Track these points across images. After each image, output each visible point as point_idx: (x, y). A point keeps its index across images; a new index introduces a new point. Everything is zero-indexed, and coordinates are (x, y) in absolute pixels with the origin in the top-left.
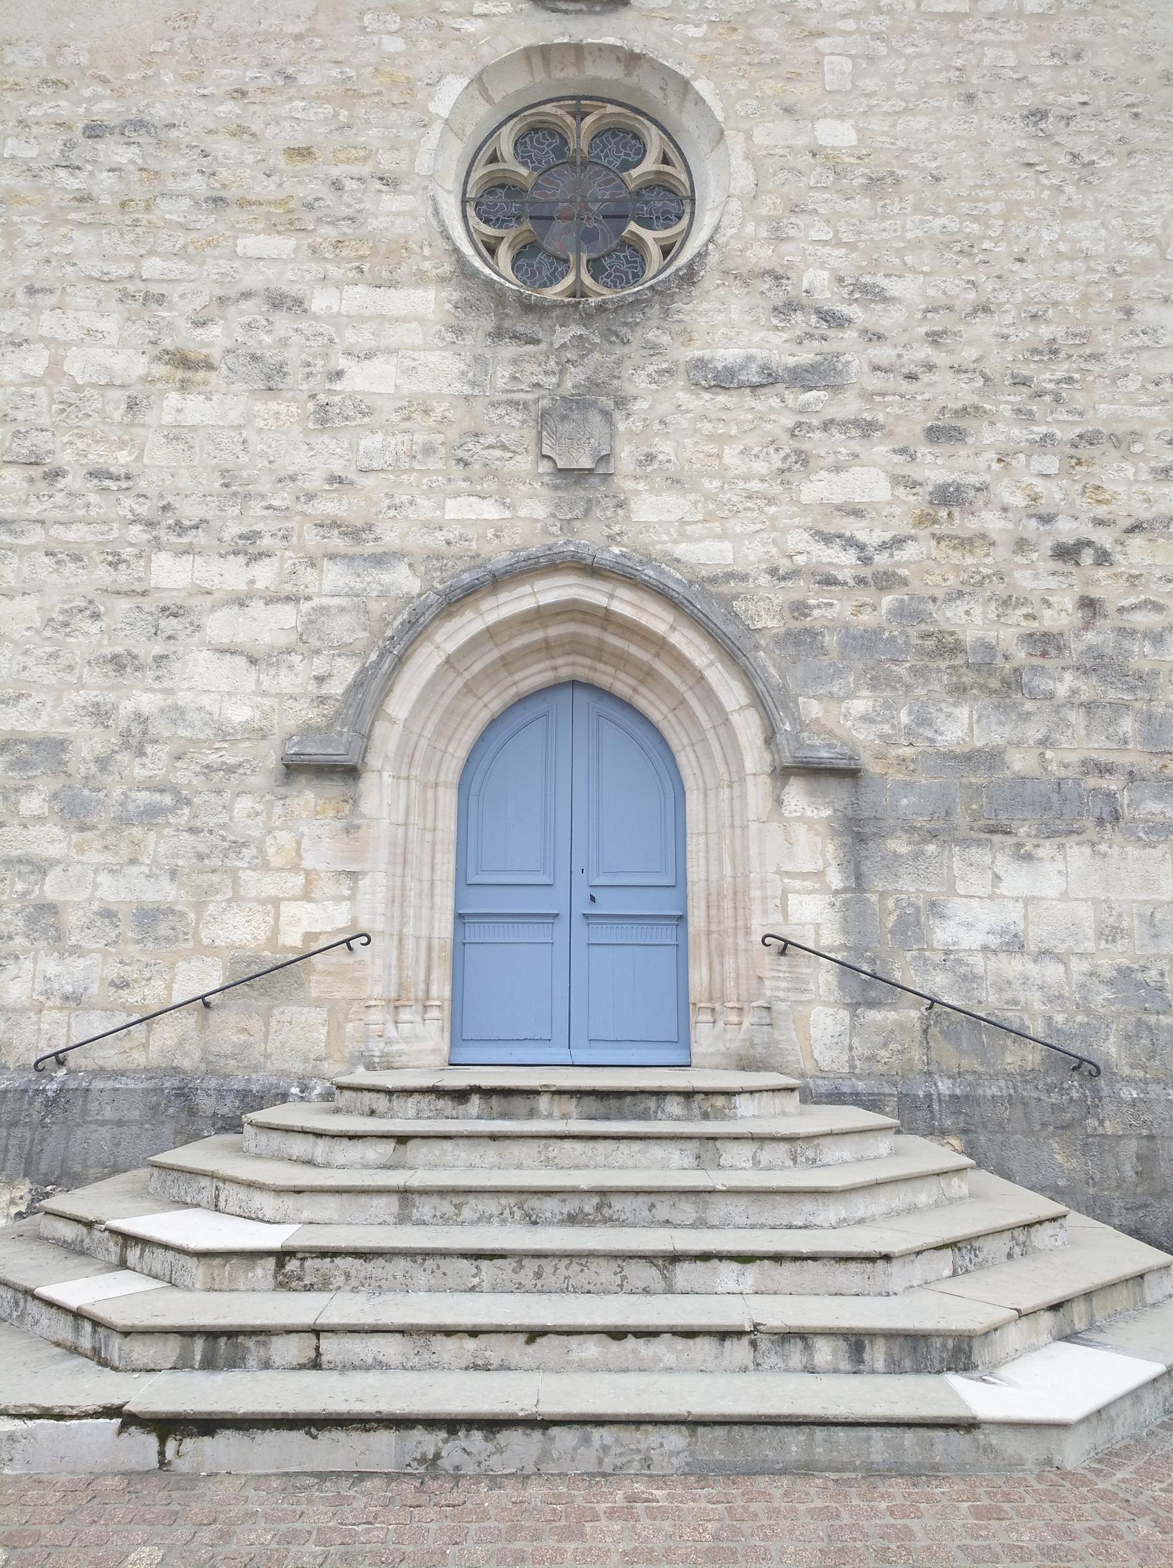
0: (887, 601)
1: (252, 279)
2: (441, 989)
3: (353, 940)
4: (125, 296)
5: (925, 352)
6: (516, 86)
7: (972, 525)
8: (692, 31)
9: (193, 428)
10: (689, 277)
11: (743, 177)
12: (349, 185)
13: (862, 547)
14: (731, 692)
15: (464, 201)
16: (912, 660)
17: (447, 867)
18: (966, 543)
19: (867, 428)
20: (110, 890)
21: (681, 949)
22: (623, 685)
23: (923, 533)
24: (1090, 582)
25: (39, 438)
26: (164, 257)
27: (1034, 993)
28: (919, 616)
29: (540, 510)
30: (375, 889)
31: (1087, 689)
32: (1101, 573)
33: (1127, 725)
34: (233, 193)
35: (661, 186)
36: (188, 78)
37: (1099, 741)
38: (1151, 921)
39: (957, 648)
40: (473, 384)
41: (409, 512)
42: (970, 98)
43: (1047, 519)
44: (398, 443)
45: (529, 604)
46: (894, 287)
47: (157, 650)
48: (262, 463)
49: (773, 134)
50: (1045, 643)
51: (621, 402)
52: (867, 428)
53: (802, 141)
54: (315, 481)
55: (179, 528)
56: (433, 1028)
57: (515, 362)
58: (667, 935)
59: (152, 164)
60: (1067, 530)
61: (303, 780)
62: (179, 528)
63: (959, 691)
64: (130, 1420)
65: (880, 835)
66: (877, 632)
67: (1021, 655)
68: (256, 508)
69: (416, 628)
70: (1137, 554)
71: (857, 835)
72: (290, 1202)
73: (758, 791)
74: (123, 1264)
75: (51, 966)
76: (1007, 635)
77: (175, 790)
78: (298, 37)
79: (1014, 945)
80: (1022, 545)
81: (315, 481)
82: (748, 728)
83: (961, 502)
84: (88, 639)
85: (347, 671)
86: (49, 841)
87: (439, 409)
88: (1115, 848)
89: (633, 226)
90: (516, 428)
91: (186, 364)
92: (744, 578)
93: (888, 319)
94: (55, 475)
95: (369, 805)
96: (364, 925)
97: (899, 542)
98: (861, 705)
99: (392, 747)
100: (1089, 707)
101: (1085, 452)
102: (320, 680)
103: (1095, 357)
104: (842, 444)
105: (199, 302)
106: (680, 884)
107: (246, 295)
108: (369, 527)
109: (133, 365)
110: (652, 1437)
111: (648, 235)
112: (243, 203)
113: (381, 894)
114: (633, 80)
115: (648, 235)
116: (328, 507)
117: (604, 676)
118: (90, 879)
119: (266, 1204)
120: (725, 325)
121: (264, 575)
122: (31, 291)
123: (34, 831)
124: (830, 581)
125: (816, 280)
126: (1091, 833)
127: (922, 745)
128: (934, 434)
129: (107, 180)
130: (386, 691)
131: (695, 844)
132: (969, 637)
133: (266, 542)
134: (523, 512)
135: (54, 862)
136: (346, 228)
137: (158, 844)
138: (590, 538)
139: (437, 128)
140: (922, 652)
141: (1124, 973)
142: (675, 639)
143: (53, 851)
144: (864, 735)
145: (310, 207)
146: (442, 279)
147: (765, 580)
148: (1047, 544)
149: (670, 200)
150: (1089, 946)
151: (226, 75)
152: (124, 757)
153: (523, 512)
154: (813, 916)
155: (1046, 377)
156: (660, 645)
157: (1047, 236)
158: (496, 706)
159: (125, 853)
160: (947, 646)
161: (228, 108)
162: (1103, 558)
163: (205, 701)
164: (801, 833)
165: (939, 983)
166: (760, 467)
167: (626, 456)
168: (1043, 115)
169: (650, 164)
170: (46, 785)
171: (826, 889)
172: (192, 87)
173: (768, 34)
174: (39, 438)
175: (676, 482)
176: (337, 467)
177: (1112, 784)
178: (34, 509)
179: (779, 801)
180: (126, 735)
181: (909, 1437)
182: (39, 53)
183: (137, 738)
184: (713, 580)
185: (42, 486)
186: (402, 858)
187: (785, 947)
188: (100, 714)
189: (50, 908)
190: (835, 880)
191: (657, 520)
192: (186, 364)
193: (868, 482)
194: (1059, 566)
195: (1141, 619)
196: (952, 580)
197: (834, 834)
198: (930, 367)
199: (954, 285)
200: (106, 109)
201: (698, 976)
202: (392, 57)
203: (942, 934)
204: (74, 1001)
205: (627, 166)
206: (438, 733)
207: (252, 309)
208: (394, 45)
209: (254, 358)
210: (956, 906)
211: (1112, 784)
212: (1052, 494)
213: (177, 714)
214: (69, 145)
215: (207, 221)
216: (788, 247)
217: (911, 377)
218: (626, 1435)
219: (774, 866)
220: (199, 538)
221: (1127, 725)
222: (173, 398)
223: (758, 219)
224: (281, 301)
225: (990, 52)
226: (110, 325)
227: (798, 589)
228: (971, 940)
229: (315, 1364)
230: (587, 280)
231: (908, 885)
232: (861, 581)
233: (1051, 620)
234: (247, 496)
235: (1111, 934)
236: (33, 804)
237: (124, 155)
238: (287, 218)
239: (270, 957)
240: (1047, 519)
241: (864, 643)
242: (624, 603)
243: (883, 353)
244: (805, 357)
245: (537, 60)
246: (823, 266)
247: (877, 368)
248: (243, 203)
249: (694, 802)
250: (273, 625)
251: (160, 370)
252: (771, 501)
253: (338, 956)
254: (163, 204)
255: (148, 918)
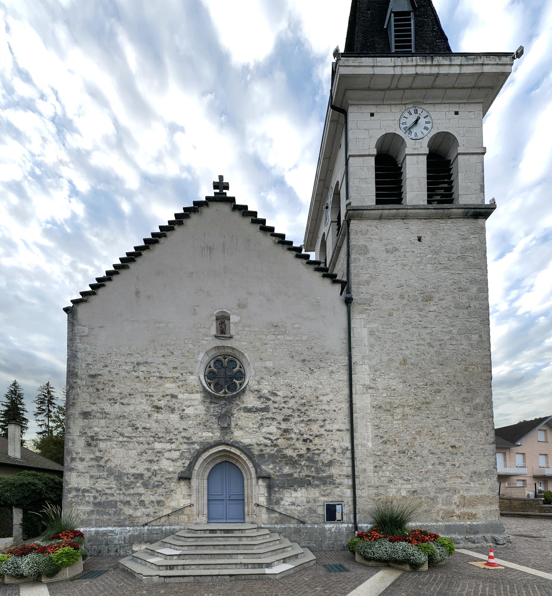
0: (275, 449)
1: (168, 392)
2: (206, 512)
3: (191, 505)
4: (146, 395)
5: (283, 405)
6: (213, 353)
7: (290, 436)
8: (244, 344)
9: (160, 420)
10: (244, 391)
11: (253, 373)
12: (184, 374)
13: (272, 440)
14: (250, 465)
15: (205, 376)
16: (279, 459)
17: (206, 492)
18: (288, 439)
19: (273, 419)
20: (152, 498)
21: (244, 504)
22: (234, 462)
23: (282, 437)
24: (309, 445)
25: (134, 422)
26: (152, 388)
27: (295, 511)
28: (281, 452)
29: (219, 434)
30: (194, 497)
31: (307, 463)
32: (310, 444)
33: (313, 469)
34: (164, 376)
35: (239, 371)
36: (154, 353)
37: (308, 472)
38: (314, 500)
39: (287, 457)
40: (207, 412)
41: (197, 435)
42: (293, 357)
43: (302, 435)
44: (195, 422)
45: (217, 450)
46: (278, 393)
47: (157, 459)
48: (172, 426)
49: (258, 364)
50: (300, 456)
51: (232, 415)
52: (273, 419)
53: (263, 365)
54: (181, 430)
55: (159, 438)
56: (204, 518)
57: (214, 408)
58: (242, 502)
59: (149, 370)
60: (305, 436)
61: (181, 480)
62: (159, 438)
63: (286, 464)
64: (160, 576)
65: (274, 487)
66: (274, 454)
67: (297, 458)
68: (171, 434)
69: (199, 454)
70: (316, 441)
71: (270, 488)
72: (180, 548)
73: (254, 481)
74: (158, 556)
75: (144, 510)
76: (294, 455)
77: (162, 482)
78: (173, 344)
79: (293, 504)
80: (298, 439)
81: (181, 430)
82: (253, 470)
83: (288, 432)
84: (145, 457)
85: (188, 462)
86: (142, 490)
87: (201, 416)
88: (310, 488)
89: (235, 380)
90: (214, 420)
91: (158, 409)
92: (252, 445)
93: (277, 399)
94: (137, 428)
95: (192, 484)
96: (192, 503)
97: (278, 439)
98: (271, 466)
99: (195, 475)
100: (307, 466)
101: (308, 423)
102: (184, 464)
103: (312, 406)
104: (269, 422)
105: (159, 397)
106: (243, 494)
107: (167, 395)
108: (190, 437)
109: (149, 409)
110: (226, 577)
111: (237, 382)
112: (166, 378)
113: (195, 498)
114: (234, 352)
115: (237, 382)
116: (183, 434)
117: (231, 460)
118: (149, 497)
119: (178, 548)
120: (250, 400)
121: (174, 446)
122: (130, 395)
123: (139, 489)
124: (266, 446)
125: (265, 392)
126: (306, 487)
127: (280, 473)
128: (284, 420)
129: (141, 373)
130: (194, 465)
131: (246, 488)
132: (288, 455)
133: (174, 440)
134: (216, 434)
135: (143, 494)
136: (184, 382)
137: (160, 490)
138: (227, 438)
139: (199, 363)
140: (281, 458)
141: (310, 508)
142: (241, 456)
143: (143, 492)
144: (271, 472)
145: (177, 378)
146: (201, 392)
147: (256, 446)
148: (302, 439)
149: (241, 375)
150: (305, 504)
151: (160, 353)
152: (153, 477)
153: (216, 434)
154: (262, 500)
155: (303, 409)
156: (239, 457)
157: (304, 384)
158: (213, 466)
159: (154, 492)
160: (285, 456)
161: (162, 359)
162: (311, 441)
163: (165, 467)
164: (261, 487)
165: (281, 510)
166: (255, 426)
167: (233, 424)
168: (305, 360)
169: (237, 368)
170: (141, 481)
171: (265, 496)
172: (155, 355)
173: (257, 344)
174: (134, 422)
175: (241, 429)
176: (185, 427)
177: (310, 479)
178: (134, 435)
179: (258, 482)
180: (153, 473)
181: (257, 576)
182: (127, 348)
183: (155, 474)
184: (247, 446)
185: (135, 430)
186: (198, 491)
187: (258, 505)
188: (148, 470)
189: (143, 501)
190: (266, 495)
191: (238, 435)
192: (158, 409)
193: (273, 429)
194: (304, 443)
195: (316, 452)
196: (286, 446)
197: (266, 487)
198: (284, 408)
199: (289, 393)
200: (140, 360)
201: (246, 509)
202: (190, 349)
203: (282, 503)
204: (148, 515)
205: (234, 368)
206: (203, 471)
207: (169, 398)
208: (191, 346)
209: (169, 407)
210: (285, 499)
211: (310, 479)
212: (303, 430)
213: (161, 470)
214: (134, 367)
215: (159, 381)
216: (260, 386)
217: (281, 410)
218: (222, 577)
219: (258, 492)
220: (163, 440)
221: (313, 469)
222: (156, 415)
223: (255, 380)
224: (173, 396)
225: (297, 348)
226: (144, 401)
227: (261, 447)
228: (287, 503)
229: (184, 569)
230: (227, 391)
231: (278, 495)
232: (271, 446)
233: (302, 452)
234: (170, 432)
235: (308, 502)
236: (138, 484)
237: (144, 369)
238: (175, 380)
239: (178, 508)
240: (302, 435)
241: (271, 456)
242: (233, 450)
243: (276, 405)
244: (263, 406)
245: (217, 349)
246: (266, 389)
247: (275, 408)
248: (166, 378)
249: (245, 481)
250: (176, 455)
251: (153, 409)
252: (257, 432)
253: (189, 508)
254: (152, 378)
255: (159, 502)
